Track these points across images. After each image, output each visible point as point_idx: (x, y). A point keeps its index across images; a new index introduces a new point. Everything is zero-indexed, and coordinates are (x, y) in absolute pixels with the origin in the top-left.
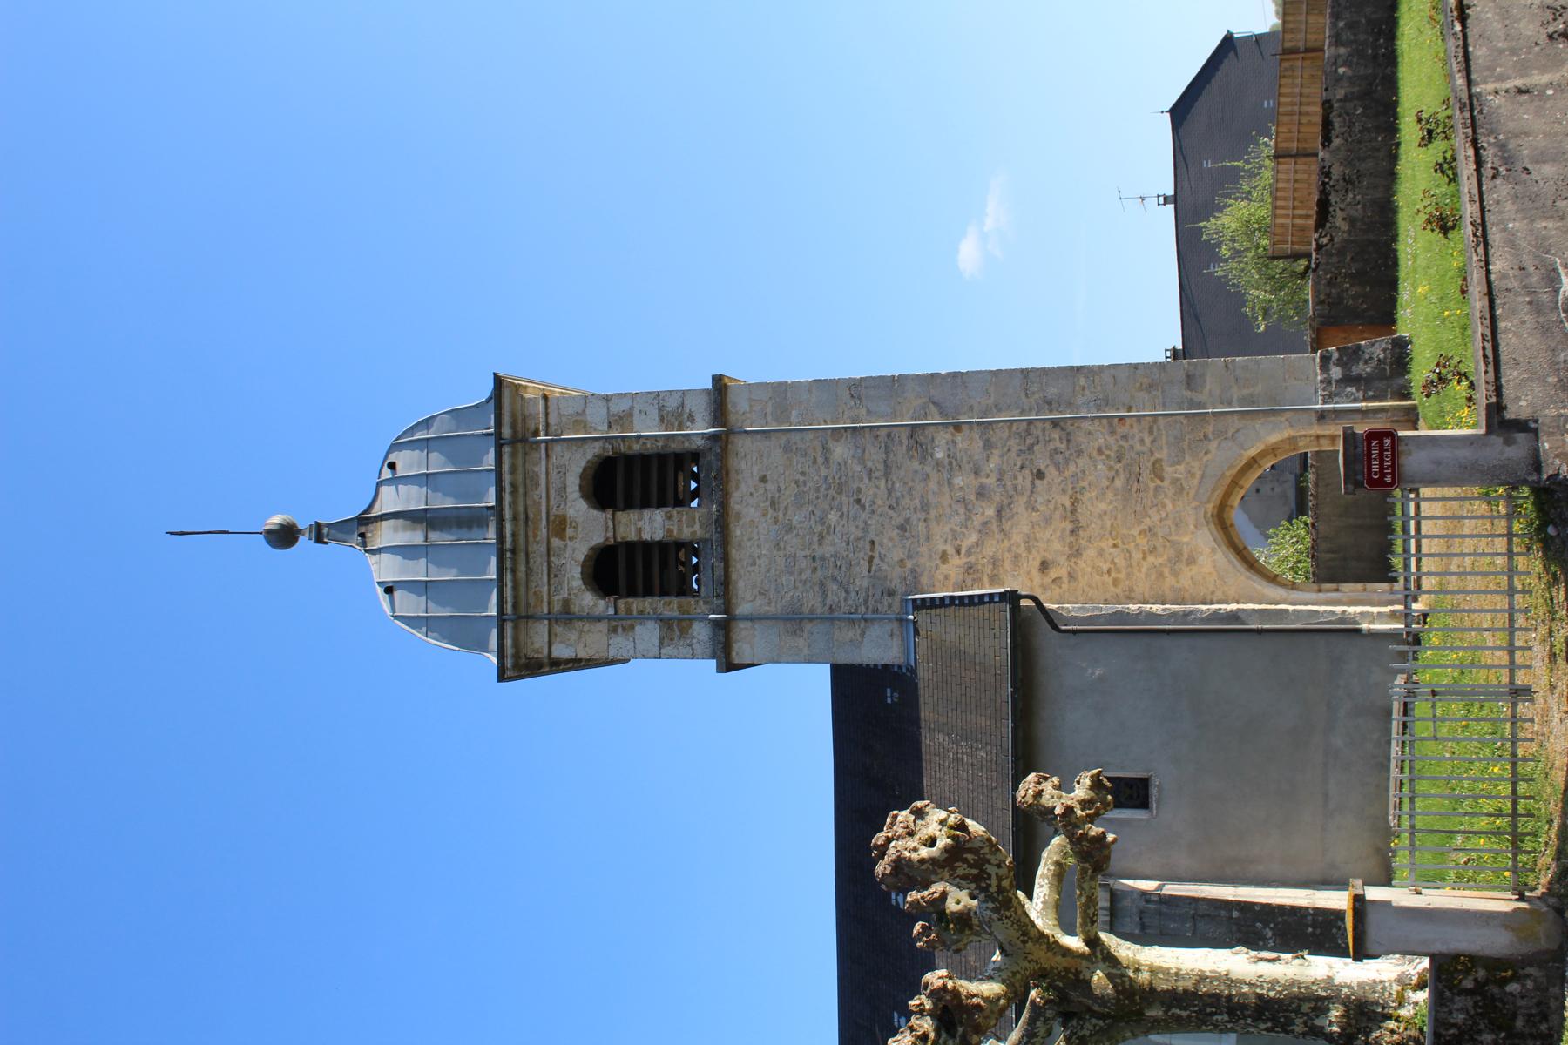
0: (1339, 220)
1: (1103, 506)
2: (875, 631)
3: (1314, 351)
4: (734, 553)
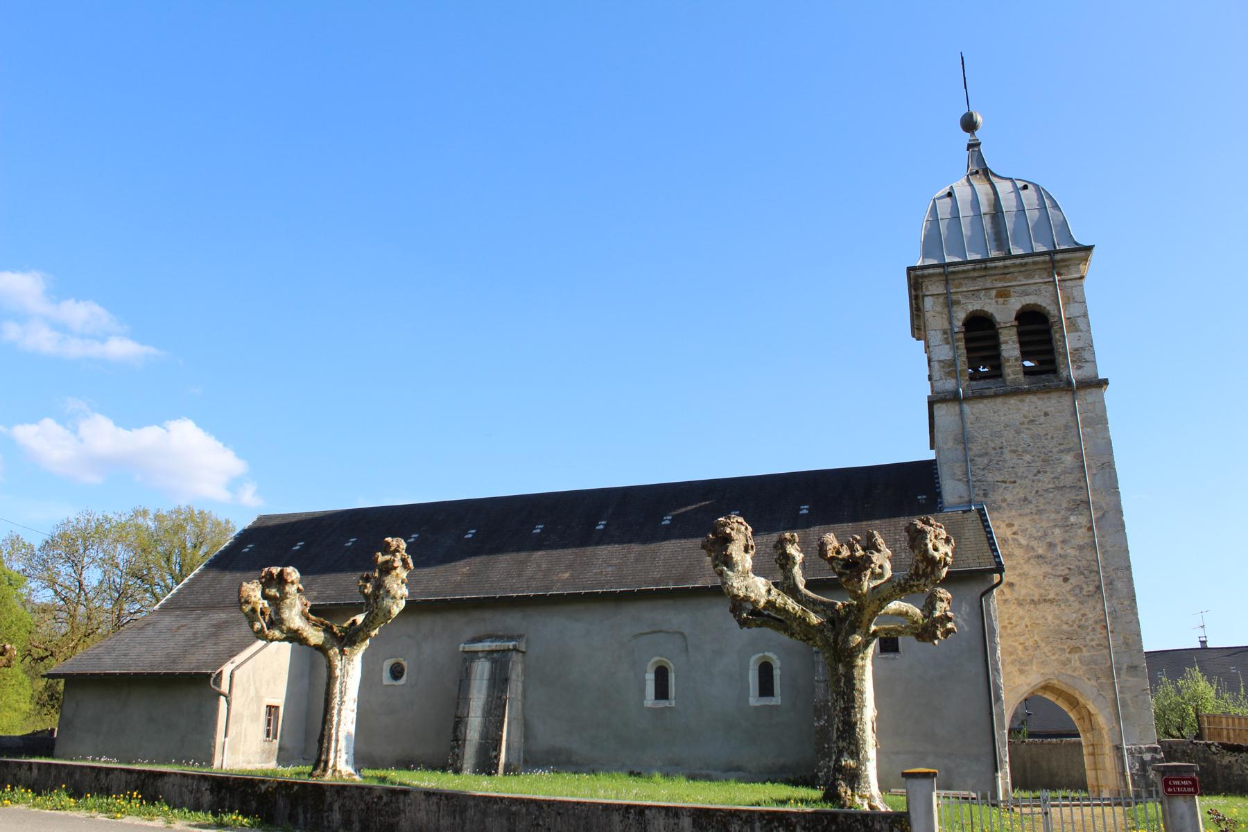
0: (1228, 758)
1: (1050, 618)
2: (961, 487)
3: (1159, 742)
4: (999, 400)
